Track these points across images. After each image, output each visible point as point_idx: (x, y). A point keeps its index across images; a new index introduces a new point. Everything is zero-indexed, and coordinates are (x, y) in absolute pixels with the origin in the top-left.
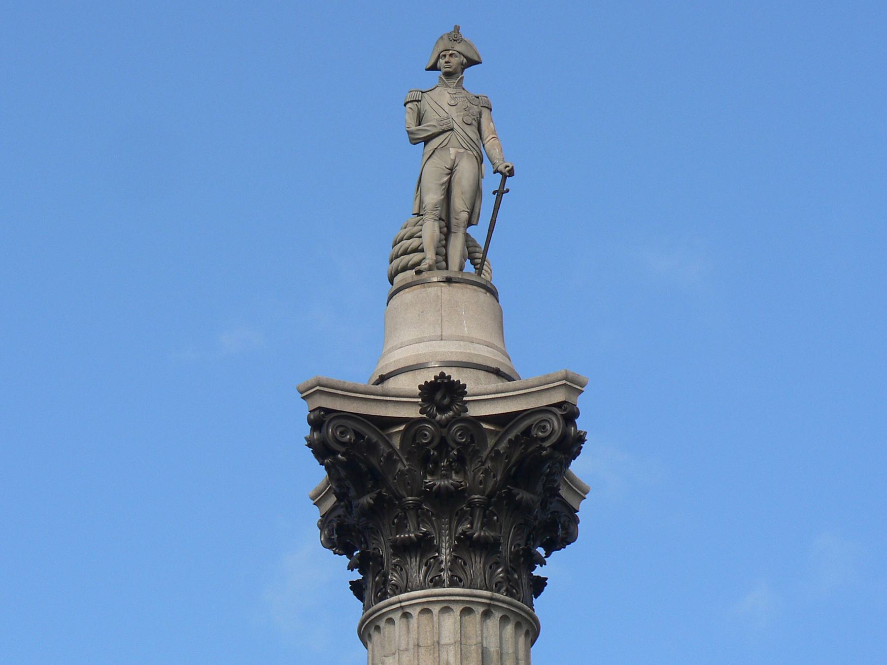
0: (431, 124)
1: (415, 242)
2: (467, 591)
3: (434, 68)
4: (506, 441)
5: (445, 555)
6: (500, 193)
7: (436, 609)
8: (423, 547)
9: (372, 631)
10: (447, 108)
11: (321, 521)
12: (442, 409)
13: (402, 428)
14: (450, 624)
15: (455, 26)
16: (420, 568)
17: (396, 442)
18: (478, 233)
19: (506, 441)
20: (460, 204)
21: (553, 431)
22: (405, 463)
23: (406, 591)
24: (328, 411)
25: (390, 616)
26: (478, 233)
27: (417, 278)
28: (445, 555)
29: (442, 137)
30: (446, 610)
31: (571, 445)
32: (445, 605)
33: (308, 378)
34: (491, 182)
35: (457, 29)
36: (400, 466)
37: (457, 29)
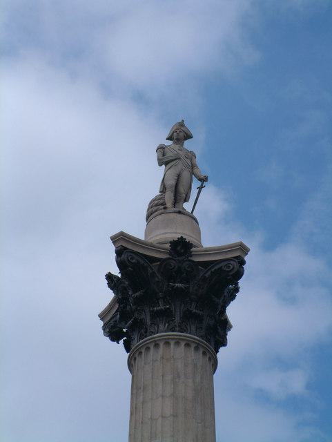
0: (169, 155)
1: (161, 201)
2: (188, 335)
3: (170, 138)
4: (209, 272)
5: (177, 319)
6: (200, 189)
7: (172, 343)
8: (166, 315)
9: (136, 355)
10: (177, 150)
11: (104, 326)
12: (180, 255)
13: (158, 263)
14: (179, 352)
15: (182, 124)
16: (181, 305)
17: (155, 270)
18: (187, 206)
19: (209, 272)
20: (182, 189)
21: (234, 268)
22: (160, 277)
23: (157, 333)
24: (125, 248)
25: (147, 345)
26: (187, 206)
27: (163, 210)
28: (177, 319)
29: (175, 162)
30: (177, 343)
31: (239, 274)
32: (177, 340)
33: (115, 232)
34: (196, 184)
35: (183, 121)
36: (157, 279)
37: (183, 121)
